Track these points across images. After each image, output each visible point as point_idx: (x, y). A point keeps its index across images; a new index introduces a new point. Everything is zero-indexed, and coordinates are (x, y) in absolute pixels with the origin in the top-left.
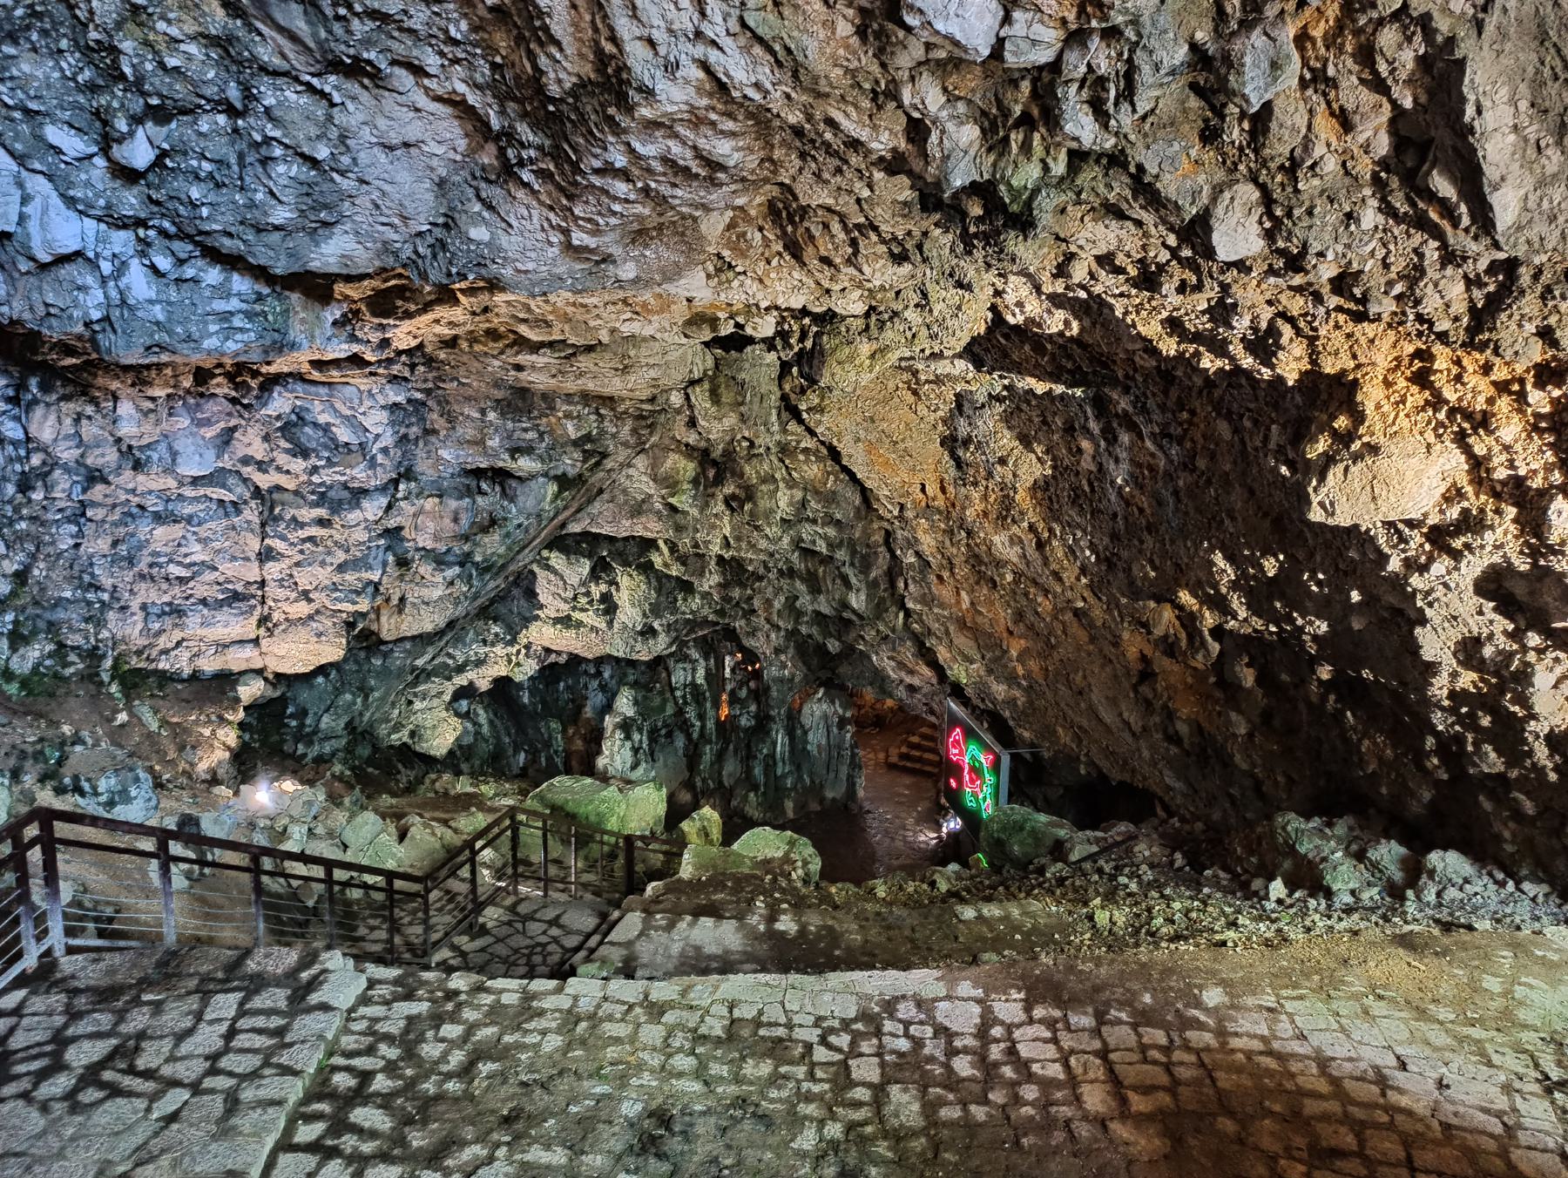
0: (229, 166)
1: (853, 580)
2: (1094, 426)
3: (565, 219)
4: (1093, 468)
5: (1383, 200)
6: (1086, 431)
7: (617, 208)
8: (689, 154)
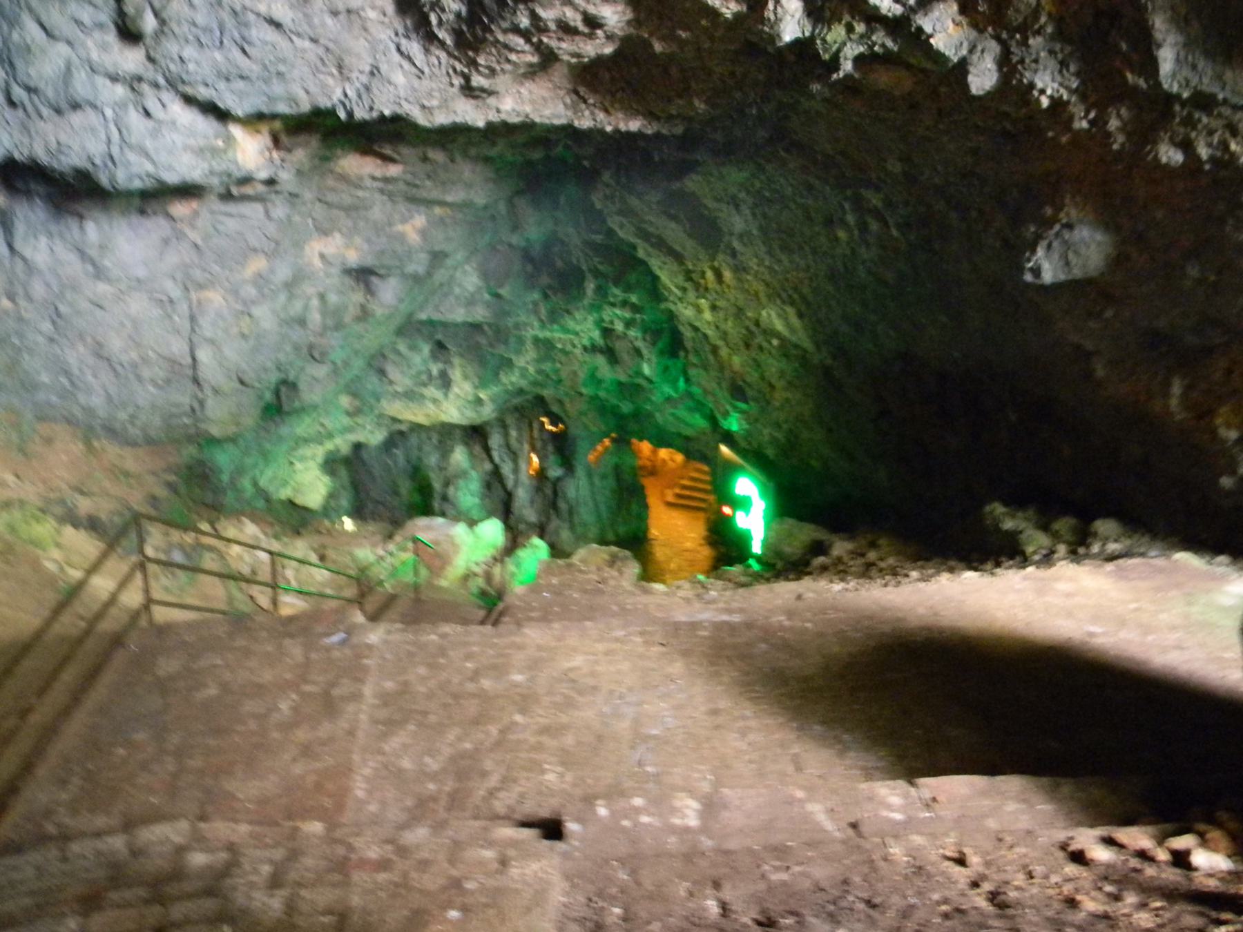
0: (211, 31)
1: (645, 352)
2: (850, 219)
3: (468, 66)
4: (848, 252)
5: (498, 789)
6: (843, 223)
7: (513, 57)
8: (579, 17)
